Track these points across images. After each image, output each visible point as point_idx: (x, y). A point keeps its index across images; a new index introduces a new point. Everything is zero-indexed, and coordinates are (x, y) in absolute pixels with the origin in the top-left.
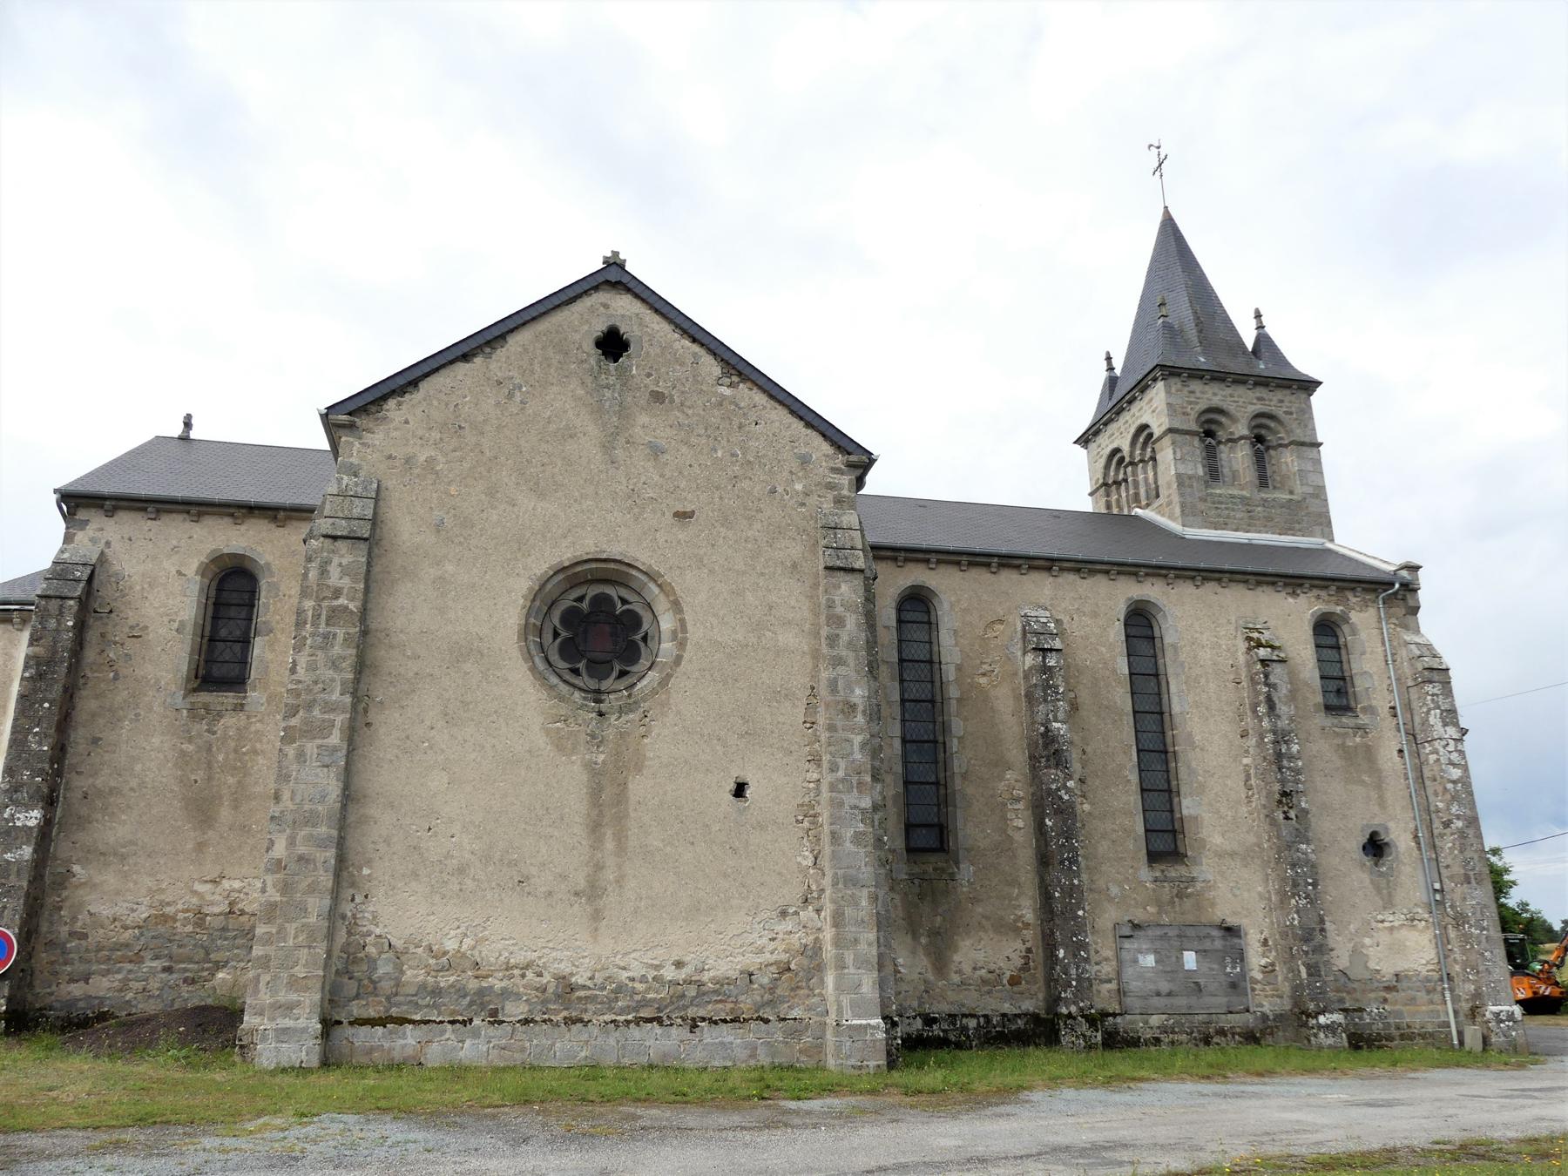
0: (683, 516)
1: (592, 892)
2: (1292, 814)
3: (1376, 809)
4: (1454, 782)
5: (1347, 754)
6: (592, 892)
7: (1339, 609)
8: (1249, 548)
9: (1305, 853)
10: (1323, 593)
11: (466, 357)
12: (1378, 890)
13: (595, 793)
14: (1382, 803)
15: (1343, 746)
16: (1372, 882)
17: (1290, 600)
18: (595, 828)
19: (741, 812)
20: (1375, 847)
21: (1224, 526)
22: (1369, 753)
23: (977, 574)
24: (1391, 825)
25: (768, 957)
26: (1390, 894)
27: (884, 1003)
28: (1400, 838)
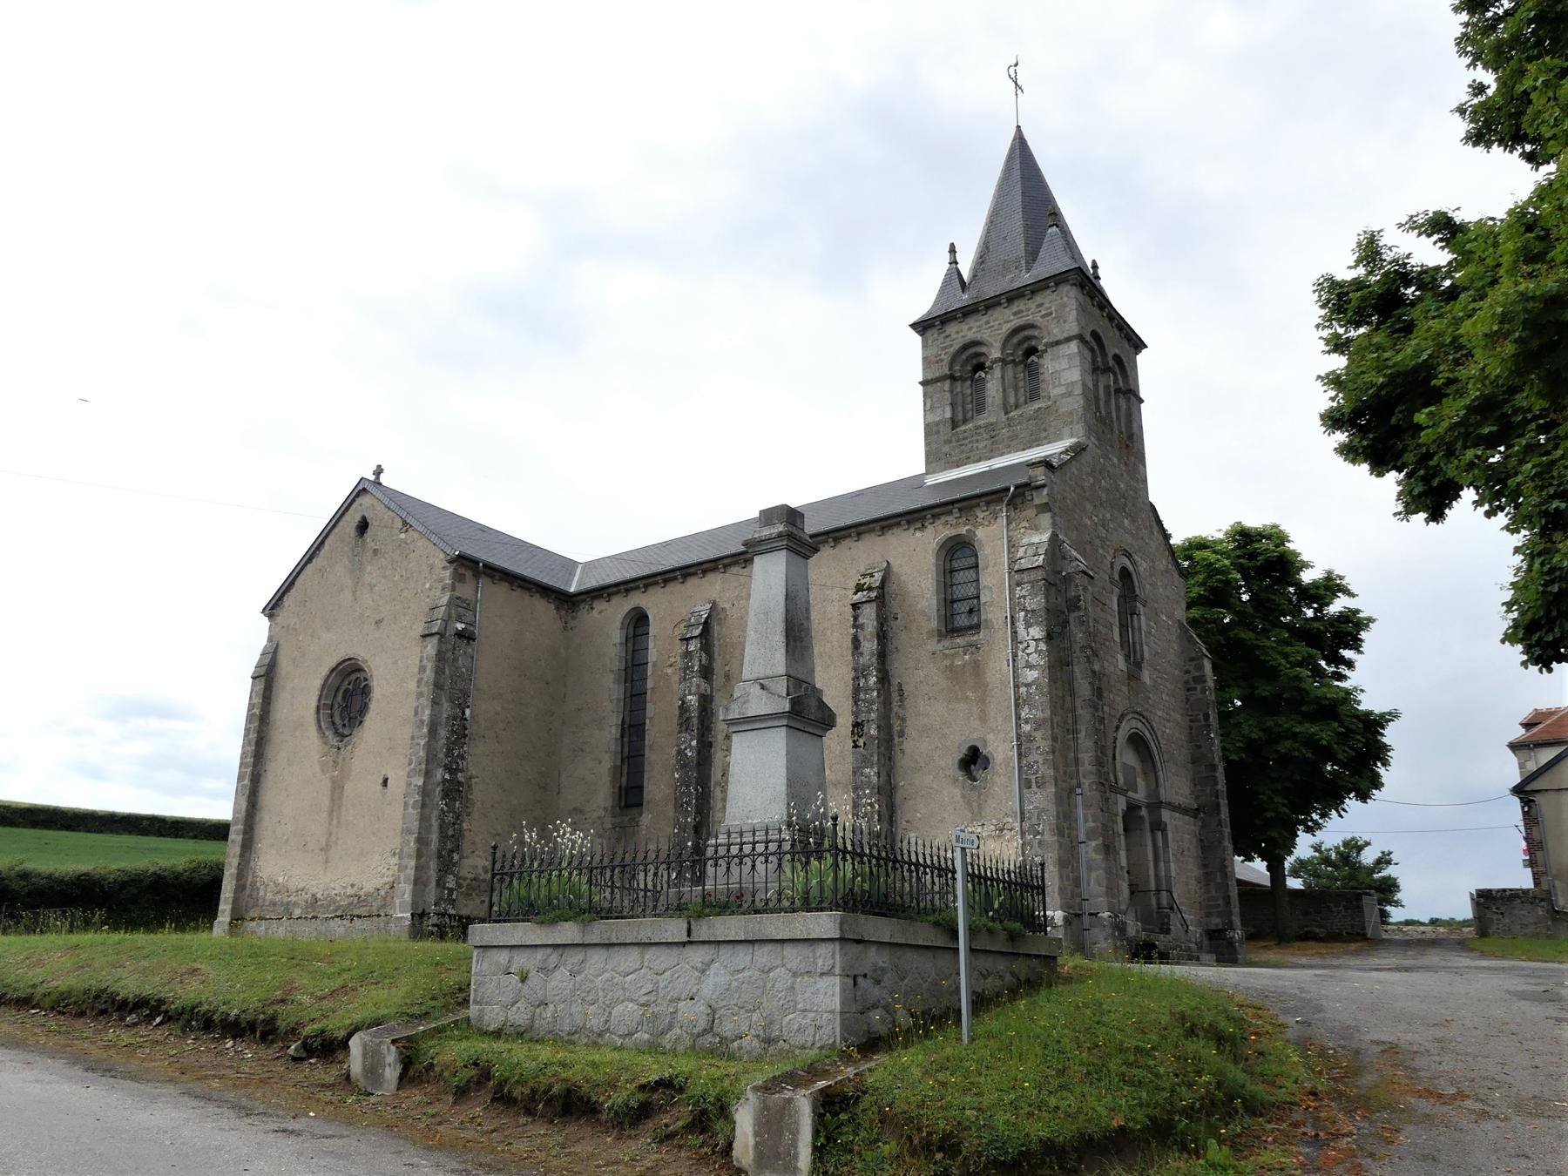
0: (378, 622)
1: (326, 849)
2: (861, 742)
3: (976, 723)
4: (1028, 685)
5: (953, 673)
6: (326, 849)
7: (963, 530)
8: (992, 473)
9: (868, 777)
10: (951, 519)
11: (310, 560)
12: (969, 804)
13: (333, 790)
14: (983, 718)
15: (951, 668)
16: (963, 796)
17: (918, 534)
18: (331, 813)
19: (384, 795)
20: (973, 760)
21: (967, 461)
22: (977, 668)
23: (675, 587)
24: (990, 737)
25: (386, 880)
26: (980, 807)
27: (414, 904)
28: (1001, 750)
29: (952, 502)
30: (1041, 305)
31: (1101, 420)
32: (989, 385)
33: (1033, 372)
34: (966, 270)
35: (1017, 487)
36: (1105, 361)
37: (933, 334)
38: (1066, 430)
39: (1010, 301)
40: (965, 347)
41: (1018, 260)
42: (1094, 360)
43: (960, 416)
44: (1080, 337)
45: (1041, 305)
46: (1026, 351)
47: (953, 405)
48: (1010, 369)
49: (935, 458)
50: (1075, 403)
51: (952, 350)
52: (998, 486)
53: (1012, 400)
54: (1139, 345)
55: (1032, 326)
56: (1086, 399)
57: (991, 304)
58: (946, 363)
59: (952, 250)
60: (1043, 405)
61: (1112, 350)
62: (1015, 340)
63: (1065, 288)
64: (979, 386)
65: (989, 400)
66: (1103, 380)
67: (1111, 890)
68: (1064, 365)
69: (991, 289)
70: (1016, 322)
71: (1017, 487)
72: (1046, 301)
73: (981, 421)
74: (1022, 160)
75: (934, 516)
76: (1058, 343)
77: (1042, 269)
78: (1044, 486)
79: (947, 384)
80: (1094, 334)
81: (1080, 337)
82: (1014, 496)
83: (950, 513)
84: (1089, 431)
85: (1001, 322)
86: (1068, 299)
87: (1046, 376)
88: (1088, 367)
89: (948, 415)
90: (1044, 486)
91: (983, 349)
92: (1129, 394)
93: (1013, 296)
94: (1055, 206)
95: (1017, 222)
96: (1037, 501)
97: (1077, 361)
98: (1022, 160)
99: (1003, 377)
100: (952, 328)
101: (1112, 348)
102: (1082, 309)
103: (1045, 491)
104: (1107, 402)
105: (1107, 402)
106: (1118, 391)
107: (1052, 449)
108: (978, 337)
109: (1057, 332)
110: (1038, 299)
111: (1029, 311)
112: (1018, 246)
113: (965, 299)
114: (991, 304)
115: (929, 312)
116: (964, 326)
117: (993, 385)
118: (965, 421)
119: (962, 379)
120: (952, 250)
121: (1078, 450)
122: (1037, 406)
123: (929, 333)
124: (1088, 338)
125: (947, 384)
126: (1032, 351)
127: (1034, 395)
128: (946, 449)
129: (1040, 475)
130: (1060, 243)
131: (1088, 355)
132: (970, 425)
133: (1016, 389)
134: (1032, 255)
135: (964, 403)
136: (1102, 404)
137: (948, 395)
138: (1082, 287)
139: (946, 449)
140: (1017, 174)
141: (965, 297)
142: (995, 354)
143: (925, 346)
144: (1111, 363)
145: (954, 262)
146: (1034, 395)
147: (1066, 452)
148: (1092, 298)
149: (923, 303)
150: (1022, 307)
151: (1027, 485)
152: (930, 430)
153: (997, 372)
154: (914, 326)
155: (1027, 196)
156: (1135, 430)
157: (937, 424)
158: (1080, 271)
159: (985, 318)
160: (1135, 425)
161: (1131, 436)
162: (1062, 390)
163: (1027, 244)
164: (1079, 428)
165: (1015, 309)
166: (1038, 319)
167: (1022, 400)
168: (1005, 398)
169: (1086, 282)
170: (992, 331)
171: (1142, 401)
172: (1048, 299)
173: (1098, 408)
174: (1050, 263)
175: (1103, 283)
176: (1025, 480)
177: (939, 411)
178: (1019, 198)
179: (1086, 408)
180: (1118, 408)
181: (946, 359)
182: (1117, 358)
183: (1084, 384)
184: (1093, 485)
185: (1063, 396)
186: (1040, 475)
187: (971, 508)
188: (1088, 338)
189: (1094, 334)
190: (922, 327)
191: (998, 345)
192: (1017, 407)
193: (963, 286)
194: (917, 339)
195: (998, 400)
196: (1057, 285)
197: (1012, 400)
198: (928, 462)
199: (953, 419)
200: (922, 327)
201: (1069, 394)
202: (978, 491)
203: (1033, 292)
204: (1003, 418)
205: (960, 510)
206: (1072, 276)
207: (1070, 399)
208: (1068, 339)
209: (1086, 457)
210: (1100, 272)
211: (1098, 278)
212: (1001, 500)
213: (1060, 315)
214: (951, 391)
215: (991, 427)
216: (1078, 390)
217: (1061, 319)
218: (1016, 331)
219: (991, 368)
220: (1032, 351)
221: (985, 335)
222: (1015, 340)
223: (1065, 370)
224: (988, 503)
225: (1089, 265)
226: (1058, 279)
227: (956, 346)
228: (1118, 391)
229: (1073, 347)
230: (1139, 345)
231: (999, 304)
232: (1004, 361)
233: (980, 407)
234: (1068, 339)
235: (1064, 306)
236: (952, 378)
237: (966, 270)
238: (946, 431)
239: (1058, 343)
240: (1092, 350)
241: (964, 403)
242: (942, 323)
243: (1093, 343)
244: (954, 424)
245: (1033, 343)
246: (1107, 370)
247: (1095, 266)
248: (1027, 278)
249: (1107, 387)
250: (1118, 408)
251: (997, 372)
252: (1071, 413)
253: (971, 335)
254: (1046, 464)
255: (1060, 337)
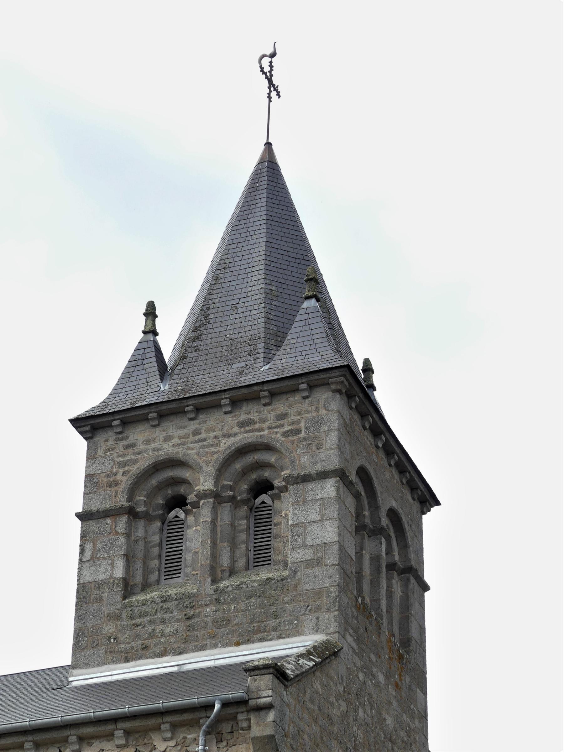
29: (115, 720)
30: (284, 416)
31: (363, 609)
32: (190, 533)
33: (262, 522)
34: (168, 343)
35: (225, 704)
36: (375, 518)
37: (107, 439)
38: (309, 620)
39: (235, 403)
40: (158, 466)
41: (252, 343)
42: (359, 515)
43: (138, 578)
44: (341, 475)
45: (284, 416)
46: (254, 487)
47: (129, 558)
48: (226, 513)
49: (89, 642)
50: (326, 578)
51: (135, 469)
52: (194, 700)
53: (225, 561)
54: (427, 499)
55: (268, 448)
56: (344, 572)
57: (206, 404)
58: (123, 488)
59: (151, 312)
60: (274, 575)
61: (387, 501)
62: (238, 466)
63: (323, 396)
64: (174, 533)
65: (188, 557)
66: (370, 546)
67: (405, 678)
68: (314, 515)
69: (206, 381)
70: (243, 438)
71: (225, 704)
72: (292, 411)
73: (173, 588)
74: (268, 176)
75: (81, 739)
76: (306, 479)
77: (293, 359)
78: (269, 707)
79: (122, 523)
80: (362, 472)
81: (341, 475)
82: (219, 719)
83: (110, 736)
84: (345, 625)
85: (223, 433)
86: (328, 410)
87: (284, 529)
88: (351, 523)
89: (119, 572)
90: (269, 707)
91: (187, 474)
92: (410, 576)
93: (242, 397)
94: (316, 270)
95: (255, 285)
96: (257, 731)
97: (333, 511)
98: (268, 176)
99: (214, 523)
100: (139, 435)
101: (389, 495)
102: (346, 430)
103: (271, 716)
104: (375, 583)
105: (375, 583)
106: (391, 567)
107: (287, 648)
108: (180, 453)
109: (306, 463)
110: (280, 406)
111: (263, 422)
112: (251, 318)
113: (164, 390)
114: (206, 404)
115: (104, 404)
116: (159, 434)
117: (196, 535)
118: (145, 586)
119: (148, 517)
120: (151, 312)
121: (326, 655)
122: (264, 575)
123: (100, 437)
124: (353, 477)
125: (122, 523)
126: (264, 487)
127: (261, 556)
128: (110, 628)
129: (265, 689)
130: (319, 326)
131: (350, 501)
132: (154, 594)
133: (234, 546)
134: (276, 339)
135: (146, 558)
136: (366, 587)
137: (122, 539)
138: (350, 396)
139: (110, 628)
140: (260, 213)
141: (165, 387)
142: (205, 483)
143: (91, 456)
144: (385, 521)
145: (151, 331)
146: (261, 556)
147: (307, 655)
148: (363, 416)
149: (95, 391)
150: (255, 416)
151: (241, 703)
152: (85, 595)
153: (205, 512)
154: (77, 422)
155: (270, 244)
156: (414, 633)
157: (99, 585)
158: (349, 369)
159: (194, 425)
160: (414, 626)
161: (406, 642)
162: (308, 554)
163: (268, 320)
164: (330, 620)
165: (243, 417)
166: (277, 437)
167: (241, 563)
168: (214, 556)
169: (355, 386)
170: (203, 448)
171: (426, 588)
172: (298, 410)
173: (360, 591)
174: (301, 354)
175: (379, 396)
176: (237, 694)
177: (105, 565)
178: (262, 249)
179: (342, 588)
180: (390, 595)
181: (125, 481)
182: (393, 514)
183: (342, 549)
184: (344, 715)
185: (309, 564)
186: (265, 689)
187: (146, 732)
188: (353, 477)
189: (362, 472)
190: (89, 425)
191: (211, 470)
192: (232, 572)
193: (163, 369)
194: (80, 444)
195: (204, 559)
196: (311, 387)
197: (225, 561)
198: (77, 647)
199: (126, 582)
200: (89, 425)
201: (318, 562)
202: (159, 705)
203: (273, 395)
204: (209, 588)
205: (128, 733)
206: (337, 378)
207: (317, 571)
208: (323, 475)
209: (338, 668)
210: (376, 379)
211: (372, 387)
212: (194, 724)
213: (314, 435)
214: (128, 535)
215: (187, 602)
216: (332, 558)
217: (313, 443)
218: (242, 451)
219: (196, 505)
220: (264, 487)
221: (192, 453)
222: (238, 466)
223: (313, 523)
224: (174, 727)
225: (360, 366)
226: (311, 381)
227: (143, 463)
228: (391, 567)
229: (329, 488)
230: (427, 499)
231: (218, 406)
232: (217, 497)
233: (172, 566)
234: (323, 475)
235: (318, 422)
236: (132, 513)
237: (168, 343)
238: (112, 599)
239: (306, 479)
240: (357, 496)
241: (146, 558)
242: (125, 423)
243: (359, 485)
244: (128, 588)
245: (267, 474)
246: (377, 532)
247: (368, 369)
248: (264, 372)
249: (375, 559)
250: (390, 595)
251: (205, 512)
252: (318, 594)
253: (168, 449)
254: (276, 670)
255: (310, 470)
